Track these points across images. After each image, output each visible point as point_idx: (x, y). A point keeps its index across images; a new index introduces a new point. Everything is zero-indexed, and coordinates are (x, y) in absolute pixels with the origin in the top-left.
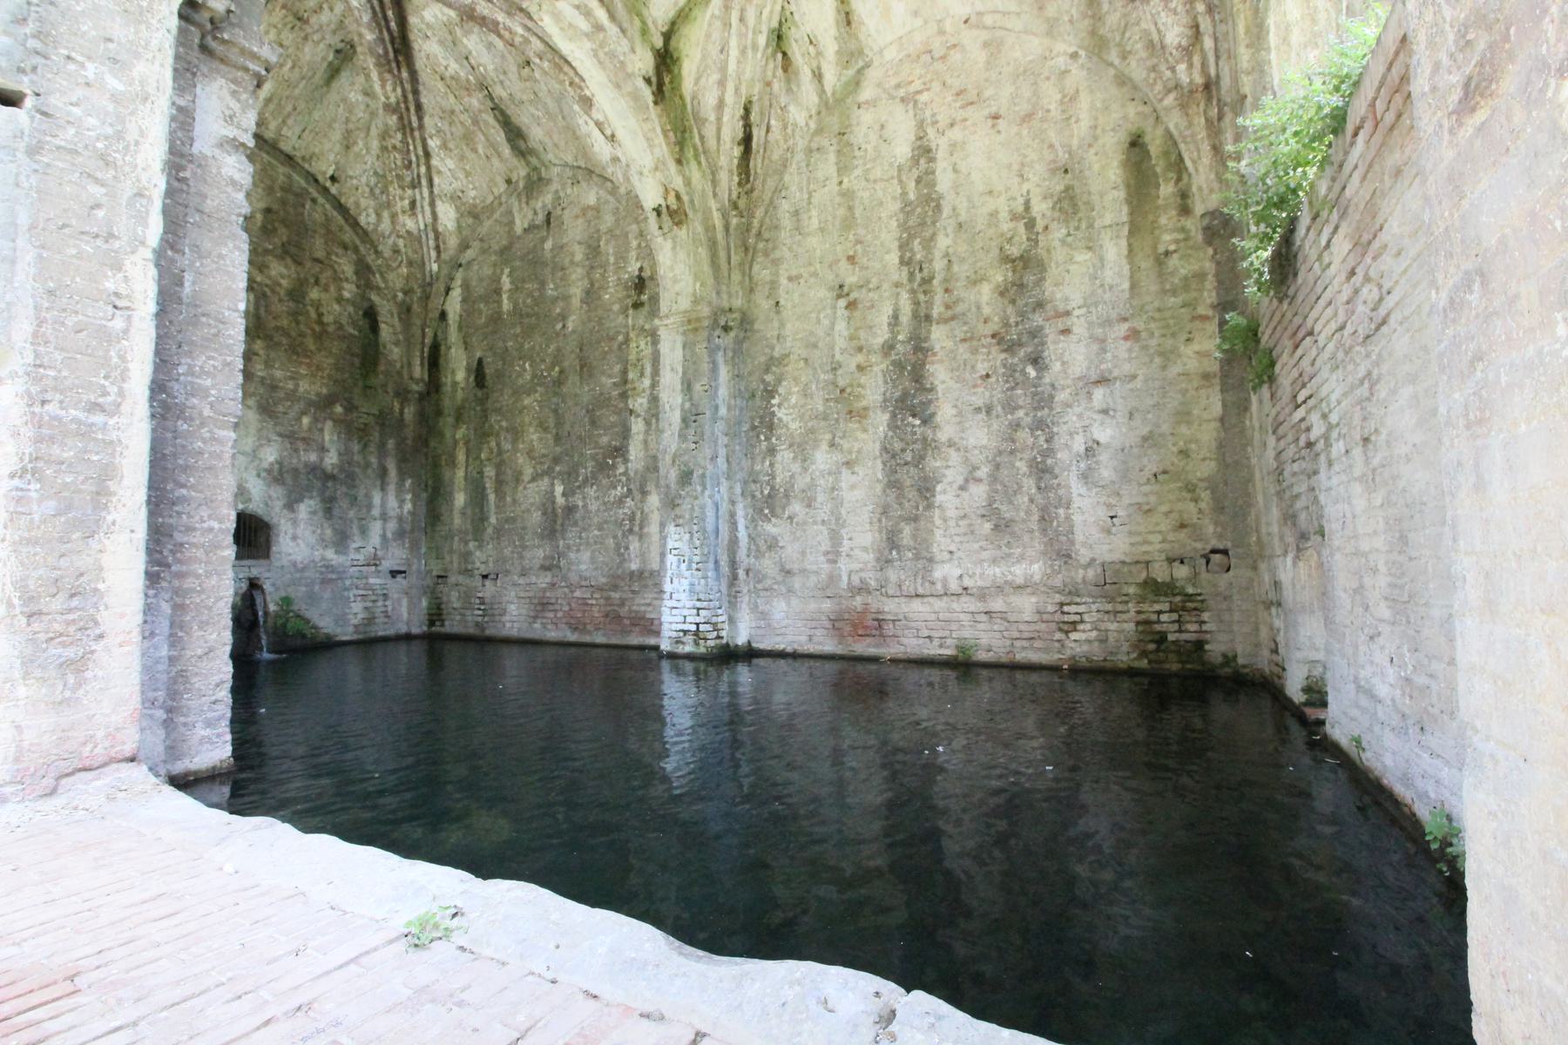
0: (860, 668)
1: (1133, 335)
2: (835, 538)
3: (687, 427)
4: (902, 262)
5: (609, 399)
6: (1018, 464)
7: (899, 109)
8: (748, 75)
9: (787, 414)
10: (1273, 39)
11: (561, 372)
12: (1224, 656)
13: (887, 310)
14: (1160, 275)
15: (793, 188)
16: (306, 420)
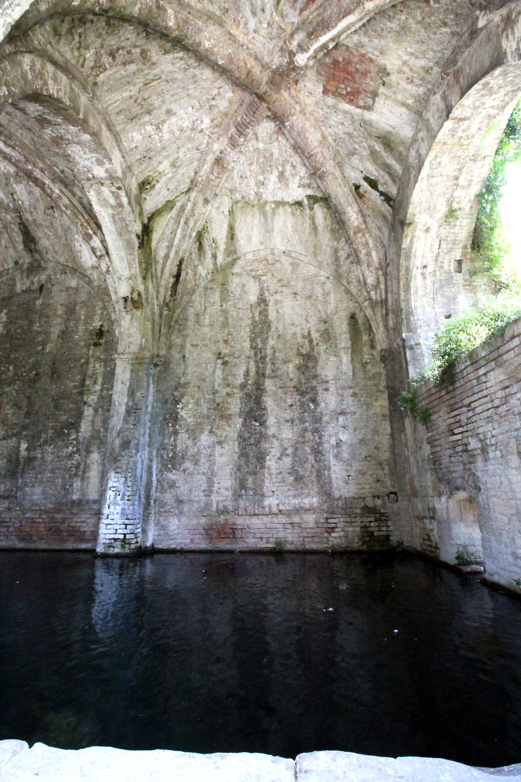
0: (221, 557)
1: (354, 395)
2: (210, 482)
4: (251, 347)
6: (306, 448)
7: (252, 281)
8: (184, 247)
9: (186, 413)
10: (412, 291)
11: (36, 375)
12: (398, 542)
13: (243, 369)
14: (364, 371)
15: (197, 303)
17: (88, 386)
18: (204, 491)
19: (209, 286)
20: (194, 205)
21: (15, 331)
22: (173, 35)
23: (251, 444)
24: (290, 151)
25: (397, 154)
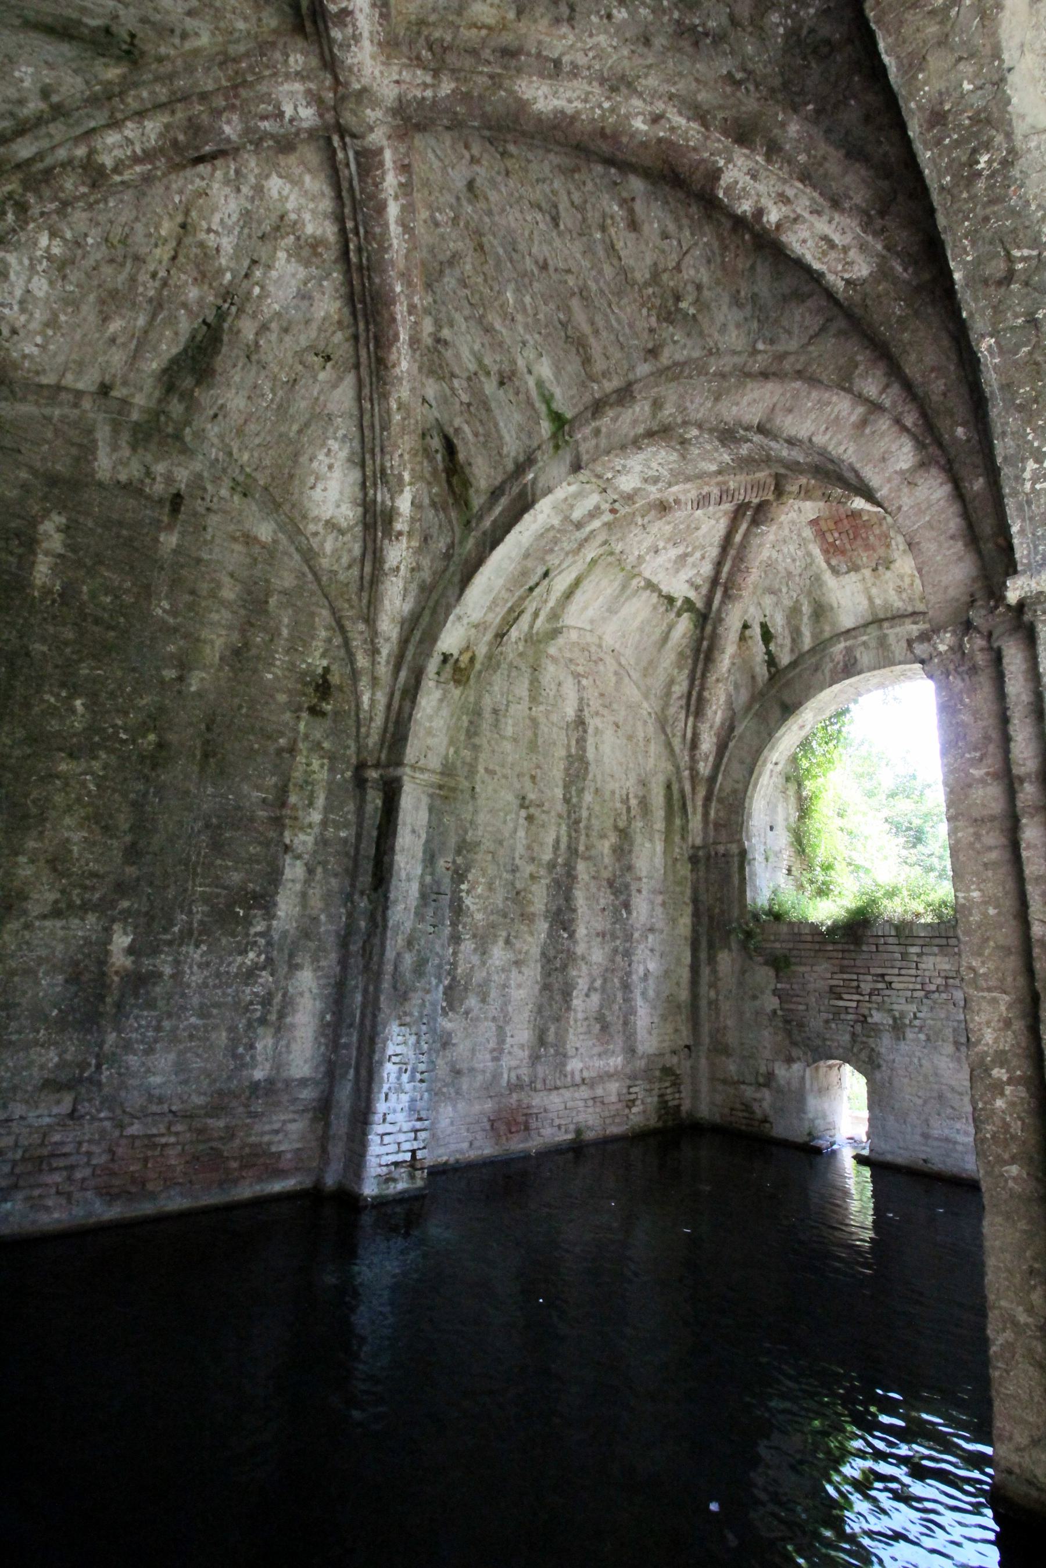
3: (425, 905)
5: (252, 820)
11: (161, 745)
17: (294, 807)
18: (494, 1050)
21: (93, 595)
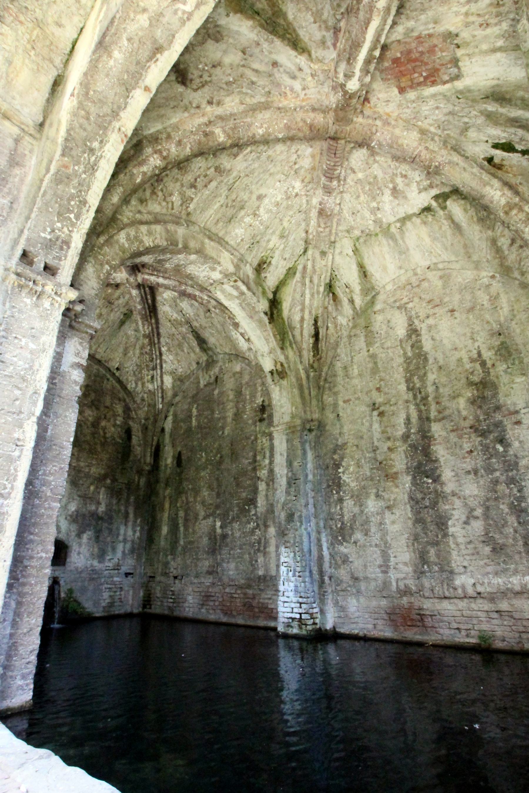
0: (411, 650)
2: (385, 556)
4: (408, 389)
6: (502, 507)
7: (397, 313)
8: (315, 305)
9: (349, 477)
11: (221, 457)
15: (343, 356)
16: (92, 488)
18: (380, 566)
19: (352, 334)
20: (314, 261)
22: (228, 145)
23: (426, 507)
24: (394, 164)
25: (519, 102)
